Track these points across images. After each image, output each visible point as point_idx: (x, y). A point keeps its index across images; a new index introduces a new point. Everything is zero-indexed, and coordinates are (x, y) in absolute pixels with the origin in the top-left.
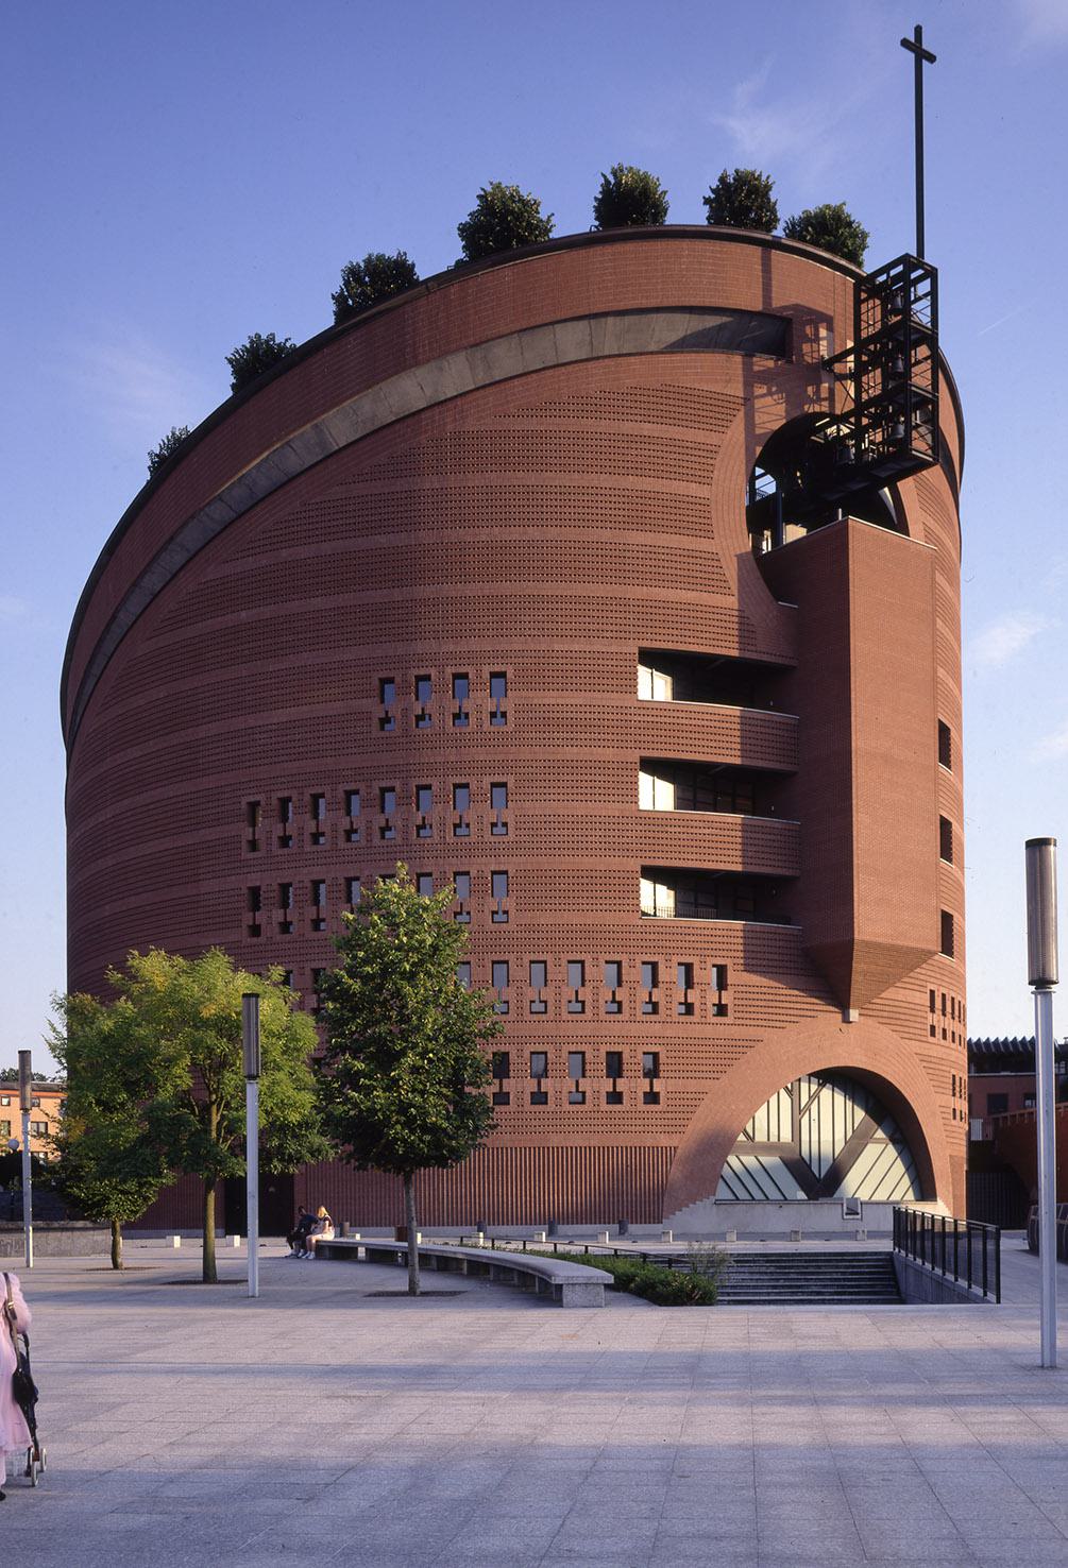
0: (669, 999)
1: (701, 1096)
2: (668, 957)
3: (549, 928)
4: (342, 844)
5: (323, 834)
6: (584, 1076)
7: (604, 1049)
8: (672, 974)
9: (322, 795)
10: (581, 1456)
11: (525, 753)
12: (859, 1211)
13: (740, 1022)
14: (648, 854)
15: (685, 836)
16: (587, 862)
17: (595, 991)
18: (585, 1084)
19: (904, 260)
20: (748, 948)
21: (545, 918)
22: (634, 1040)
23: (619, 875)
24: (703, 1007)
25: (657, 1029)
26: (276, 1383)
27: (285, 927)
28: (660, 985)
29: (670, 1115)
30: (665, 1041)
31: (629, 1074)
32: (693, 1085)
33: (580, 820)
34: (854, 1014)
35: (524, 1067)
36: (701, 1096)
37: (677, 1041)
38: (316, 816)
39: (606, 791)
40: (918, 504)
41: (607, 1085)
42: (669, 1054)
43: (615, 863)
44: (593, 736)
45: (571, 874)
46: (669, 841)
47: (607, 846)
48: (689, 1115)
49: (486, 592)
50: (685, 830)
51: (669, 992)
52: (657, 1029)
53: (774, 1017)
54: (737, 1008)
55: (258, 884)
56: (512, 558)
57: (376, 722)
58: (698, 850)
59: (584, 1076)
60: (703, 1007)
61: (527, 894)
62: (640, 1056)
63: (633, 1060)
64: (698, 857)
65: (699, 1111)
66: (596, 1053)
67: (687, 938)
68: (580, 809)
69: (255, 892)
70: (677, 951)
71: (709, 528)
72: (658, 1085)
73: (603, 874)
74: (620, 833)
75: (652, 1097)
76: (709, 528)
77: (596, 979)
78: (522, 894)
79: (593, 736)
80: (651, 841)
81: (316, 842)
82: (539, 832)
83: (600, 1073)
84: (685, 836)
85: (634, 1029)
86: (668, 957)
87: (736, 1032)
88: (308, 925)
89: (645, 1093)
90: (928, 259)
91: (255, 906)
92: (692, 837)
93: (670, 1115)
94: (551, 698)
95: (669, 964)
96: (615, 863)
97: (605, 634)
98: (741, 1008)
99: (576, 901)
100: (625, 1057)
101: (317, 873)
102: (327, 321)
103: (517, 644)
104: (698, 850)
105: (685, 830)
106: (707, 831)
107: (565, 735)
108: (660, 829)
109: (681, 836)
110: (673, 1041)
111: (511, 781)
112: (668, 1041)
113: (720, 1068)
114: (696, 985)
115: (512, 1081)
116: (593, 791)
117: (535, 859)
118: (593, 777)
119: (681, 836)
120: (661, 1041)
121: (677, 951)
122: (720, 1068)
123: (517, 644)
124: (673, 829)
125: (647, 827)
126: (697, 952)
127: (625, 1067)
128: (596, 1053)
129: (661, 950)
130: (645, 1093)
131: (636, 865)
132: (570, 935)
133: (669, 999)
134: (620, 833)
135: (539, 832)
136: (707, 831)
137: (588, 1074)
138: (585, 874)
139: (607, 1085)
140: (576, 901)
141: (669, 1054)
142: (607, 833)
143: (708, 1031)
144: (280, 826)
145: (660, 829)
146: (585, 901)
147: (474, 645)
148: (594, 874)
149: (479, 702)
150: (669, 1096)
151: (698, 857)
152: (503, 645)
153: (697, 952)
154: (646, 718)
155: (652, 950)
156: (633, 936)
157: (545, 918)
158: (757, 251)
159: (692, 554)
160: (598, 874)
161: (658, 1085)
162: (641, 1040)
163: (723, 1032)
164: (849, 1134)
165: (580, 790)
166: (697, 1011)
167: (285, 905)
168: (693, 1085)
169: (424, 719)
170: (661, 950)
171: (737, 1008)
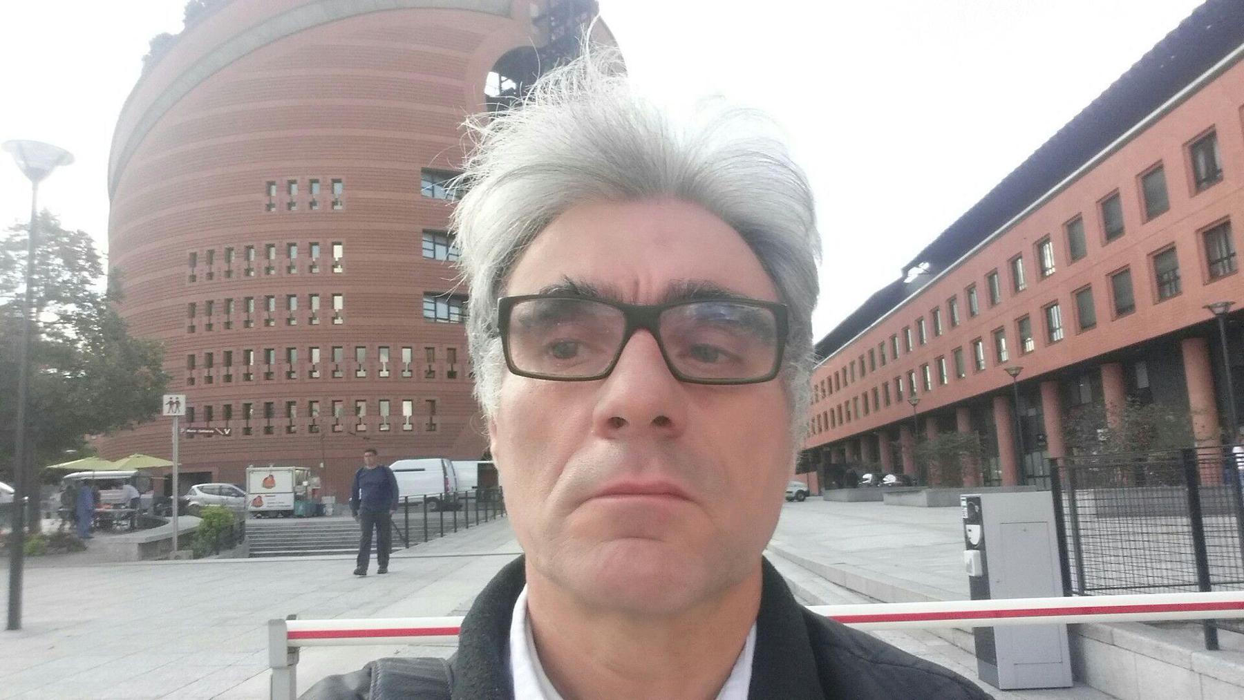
4: (243, 277)
5: (273, 268)
9: (252, 247)
10: (1169, 563)
12: (256, 496)
27: (209, 326)
31: (236, 417)
38: (229, 261)
41: (264, 423)
55: (195, 301)
57: (264, 207)
62: (424, 403)
69: (193, 305)
81: (289, 272)
88: (242, 324)
91: (192, 315)
100: (214, 408)
101: (229, 295)
115: (231, 421)
127: (233, 413)
139: (264, 423)
144: (226, 264)
166: (214, 381)
167: (210, 314)
169: (337, 204)
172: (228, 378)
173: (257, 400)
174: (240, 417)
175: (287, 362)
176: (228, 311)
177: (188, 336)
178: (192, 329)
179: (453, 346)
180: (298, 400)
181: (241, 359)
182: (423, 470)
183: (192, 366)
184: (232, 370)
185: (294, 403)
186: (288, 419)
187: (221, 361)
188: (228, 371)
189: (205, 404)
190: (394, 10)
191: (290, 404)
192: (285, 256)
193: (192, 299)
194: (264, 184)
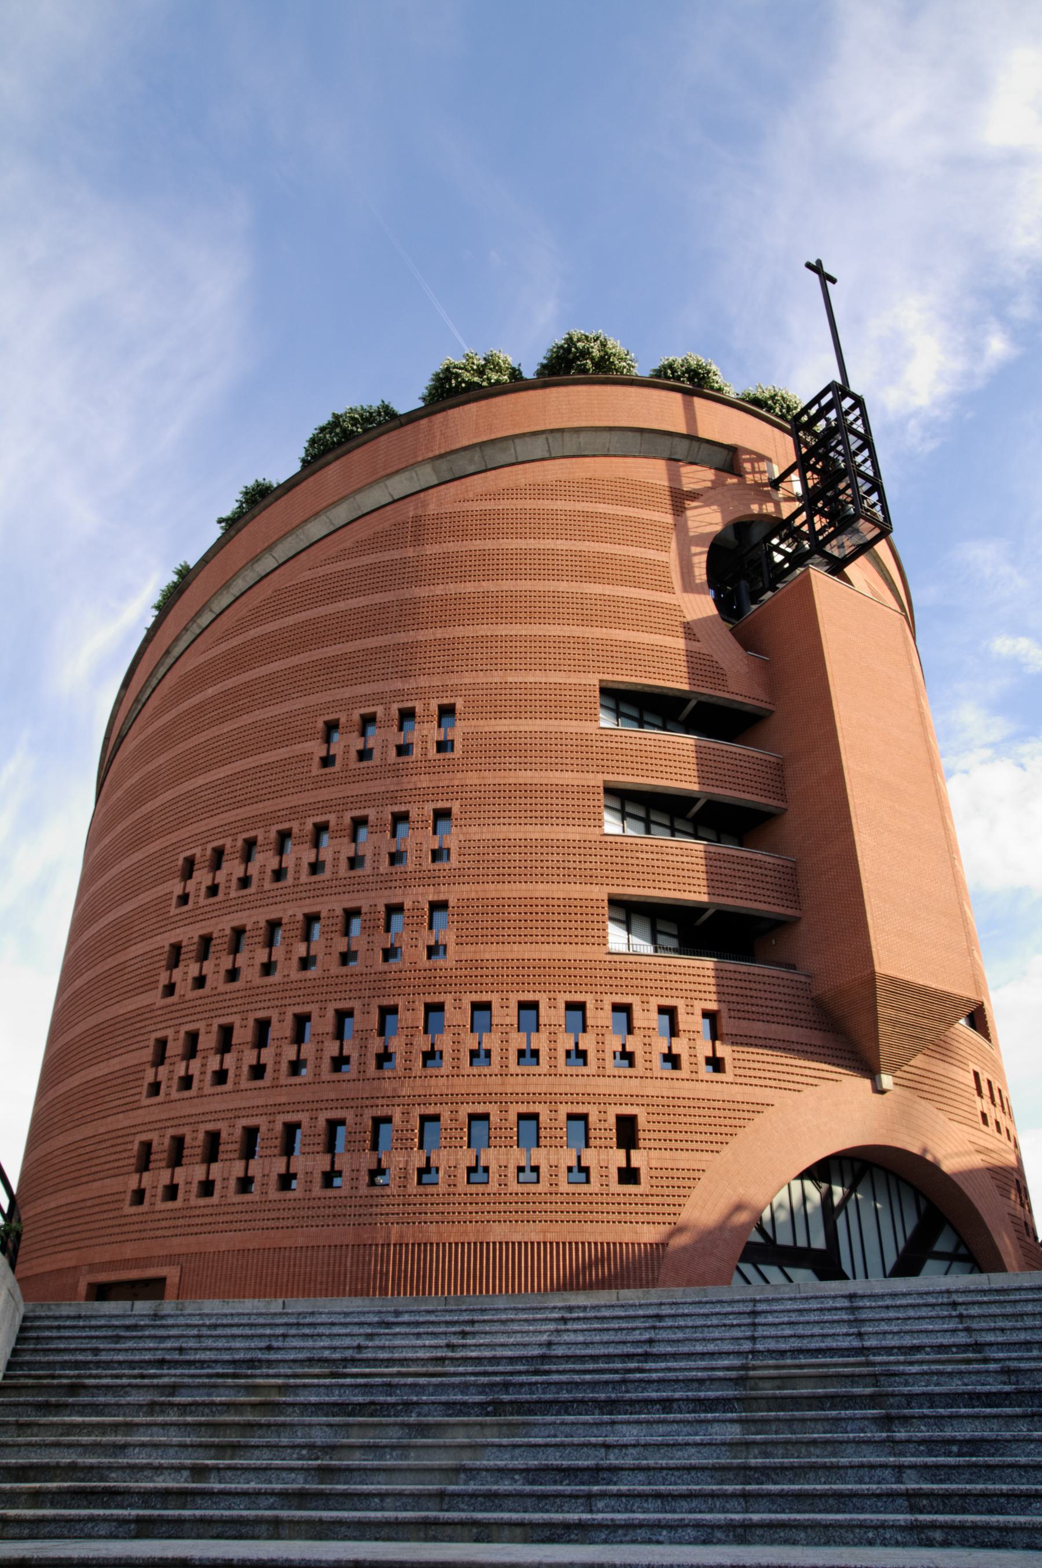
0: (647, 1049)
1: (696, 1174)
2: (645, 998)
3: (496, 964)
6: (587, 1146)
7: (613, 1112)
8: (646, 1017)
11: (472, 778)
13: (739, 1080)
14: (615, 881)
15: (660, 863)
16: (541, 890)
17: (456, 1039)
18: (590, 1158)
19: (831, 387)
20: (722, 990)
21: (490, 952)
22: (602, 1099)
23: (591, 904)
24: (693, 1060)
25: (632, 1086)
26: (82, 1530)
28: (636, 1031)
29: (655, 1200)
30: (645, 1101)
32: (685, 1160)
33: (534, 843)
34: (887, 1081)
35: (508, 1133)
36: (696, 1174)
37: (660, 1101)
39: (565, 815)
40: (715, 658)
42: (651, 1118)
43: (576, 891)
44: (549, 760)
45: (523, 902)
46: (640, 868)
47: (566, 871)
48: (682, 1200)
49: (439, 636)
50: (659, 856)
51: (647, 1040)
52: (632, 1086)
53: (752, 1073)
54: (737, 1064)
56: (467, 606)
58: (676, 879)
59: (587, 1146)
60: (693, 1060)
61: (470, 925)
63: (602, 1125)
64: (676, 886)
65: (695, 1194)
66: (602, 1116)
67: (669, 977)
68: (535, 832)
70: (653, 991)
71: (669, 585)
72: (638, 1159)
73: (561, 902)
74: (582, 858)
75: (629, 1175)
76: (669, 585)
77: (553, 1023)
78: (465, 925)
79: (549, 760)
80: (620, 867)
82: (486, 857)
83: (608, 1143)
84: (660, 863)
85: (603, 1085)
86: (645, 998)
87: (738, 1093)
89: (620, 1169)
90: (854, 388)
92: (667, 864)
93: (655, 1200)
94: (503, 725)
95: (645, 1006)
96: (576, 891)
97: (562, 668)
98: (741, 1064)
99: (528, 931)
102: (296, 467)
103: (467, 679)
104: (676, 879)
105: (659, 856)
106: (685, 859)
107: (518, 760)
108: (629, 854)
109: (655, 863)
110: (655, 1101)
111: (456, 808)
112: (650, 1101)
113: (719, 1138)
114: (681, 1033)
116: (550, 814)
117: (480, 887)
118: (549, 801)
119: (655, 863)
120: (640, 1100)
121: (653, 991)
122: (719, 1138)
123: (467, 679)
124: (644, 855)
125: (614, 852)
126: (684, 994)
127: (641, 1135)
128: (602, 1116)
129: (636, 991)
130: (620, 1169)
131: (601, 893)
132: (521, 971)
133: (647, 1049)
134: (582, 858)
135: (486, 857)
136: (685, 859)
137: (592, 1142)
138: (540, 902)
139: (618, 1157)
140: (528, 931)
141: (651, 1118)
142: (566, 857)
143: (701, 1090)
144: (277, 858)
145: (629, 854)
146: (540, 932)
147: (423, 681)
148: (550, 902)
149: (425, 732)
150: (654, 1173)
151: (676, 886)
152: (453, 680)
153: (684, 994)
154: (609, 745)
155: (624, 990)
156: (599, 973)
157: (490, 952)
158: (678, 396)
159: (652, 605)
160: (555, 902)
161: (638, 1159)
162: (612, 1099)
163: (719, 1091)
164: (901, 1244)
165: (534, 814)
168: (685, 1160)
170: (636, 991)
171: (737, 1064)
172: (258, 1071)
173: (271, 1118)
174: (316, 1148)
175: (293, 1042)
176: (307, 937)
177: (161, 1002)
178: (170, 989)
179: (578, 998)
180: (349, 1115)
181: (288, 1033)
182: (867, 1277)
183: (160, 1058)
184: (230, 1060)
185: (342, 1122)
186: (328, 1157)
187: (249, 1039)
188: (222, 1062)
189: (204, 1128)
190: (306, 521)
191: (333, 1125)
192: (346, 840)
193: (173, 937)
194: (320, 725)
